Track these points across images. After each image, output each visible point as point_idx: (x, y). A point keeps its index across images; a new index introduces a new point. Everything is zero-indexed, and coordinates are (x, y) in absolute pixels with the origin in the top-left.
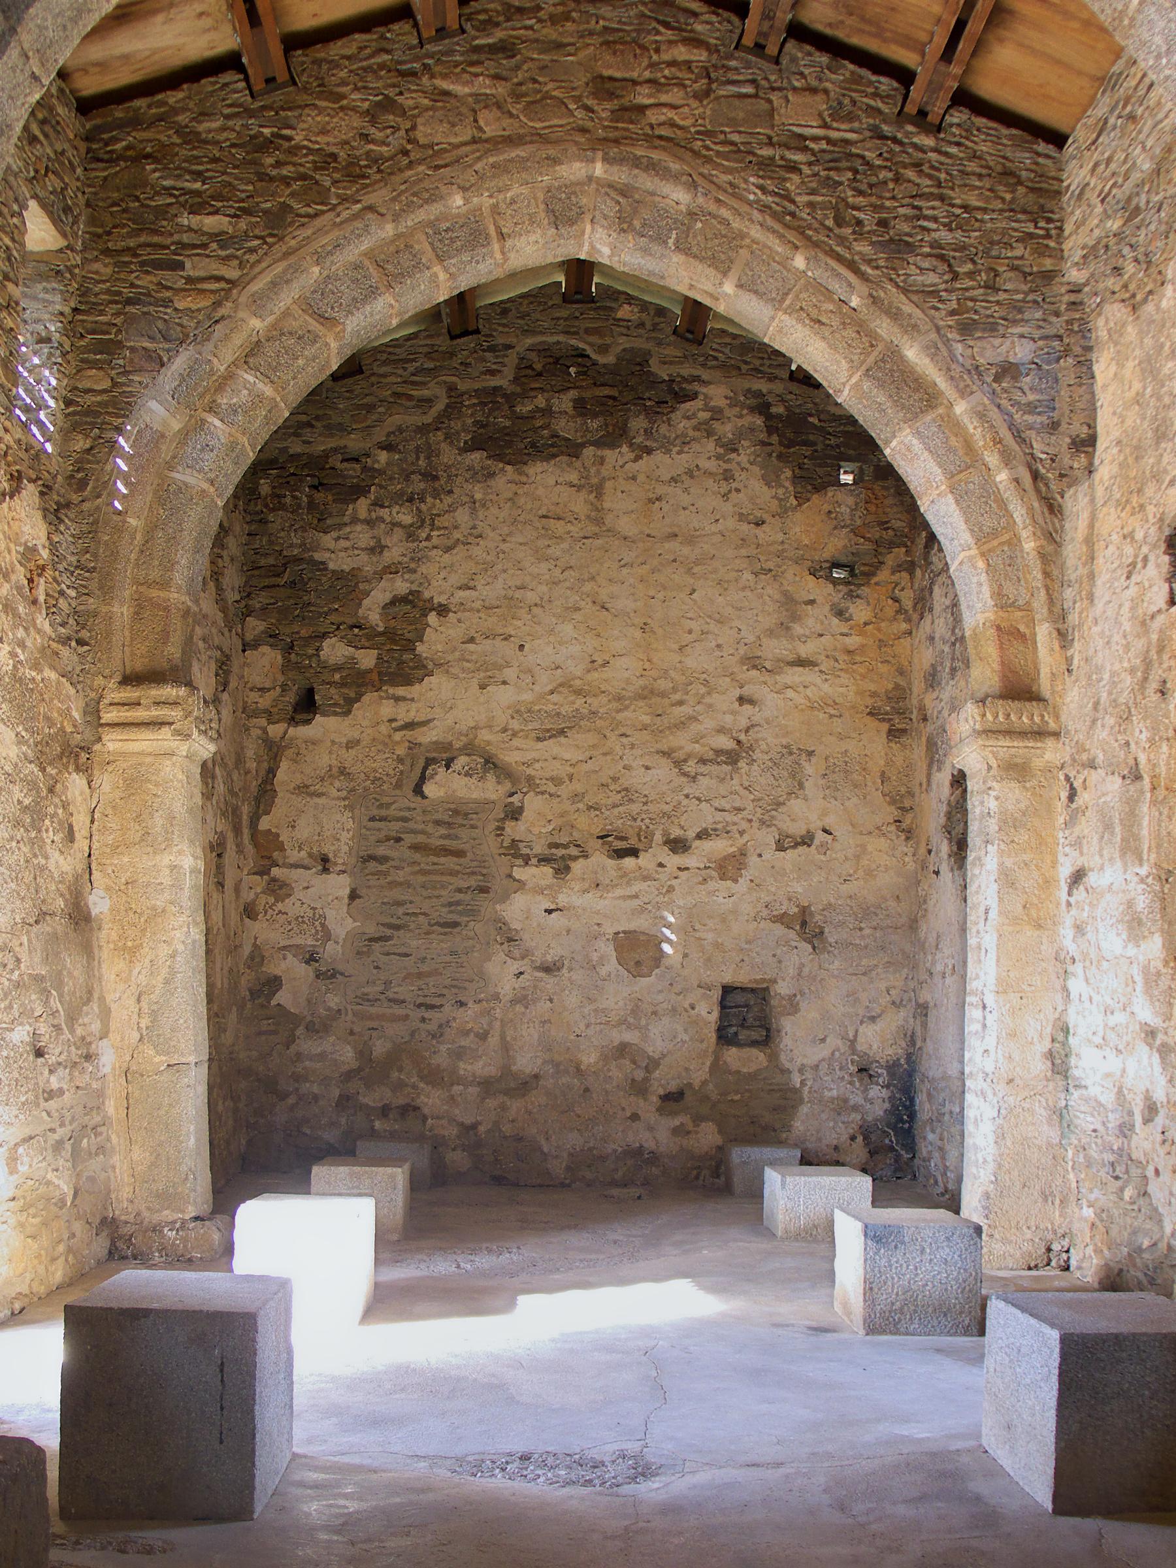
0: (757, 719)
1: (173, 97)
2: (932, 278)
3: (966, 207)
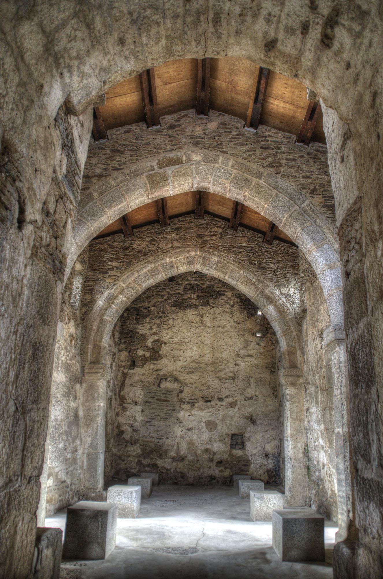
0: (239, 369)
1: (108, 238)
2: (271, 275)
3: (278, 260)
